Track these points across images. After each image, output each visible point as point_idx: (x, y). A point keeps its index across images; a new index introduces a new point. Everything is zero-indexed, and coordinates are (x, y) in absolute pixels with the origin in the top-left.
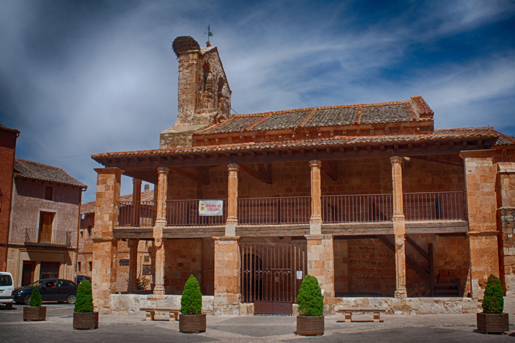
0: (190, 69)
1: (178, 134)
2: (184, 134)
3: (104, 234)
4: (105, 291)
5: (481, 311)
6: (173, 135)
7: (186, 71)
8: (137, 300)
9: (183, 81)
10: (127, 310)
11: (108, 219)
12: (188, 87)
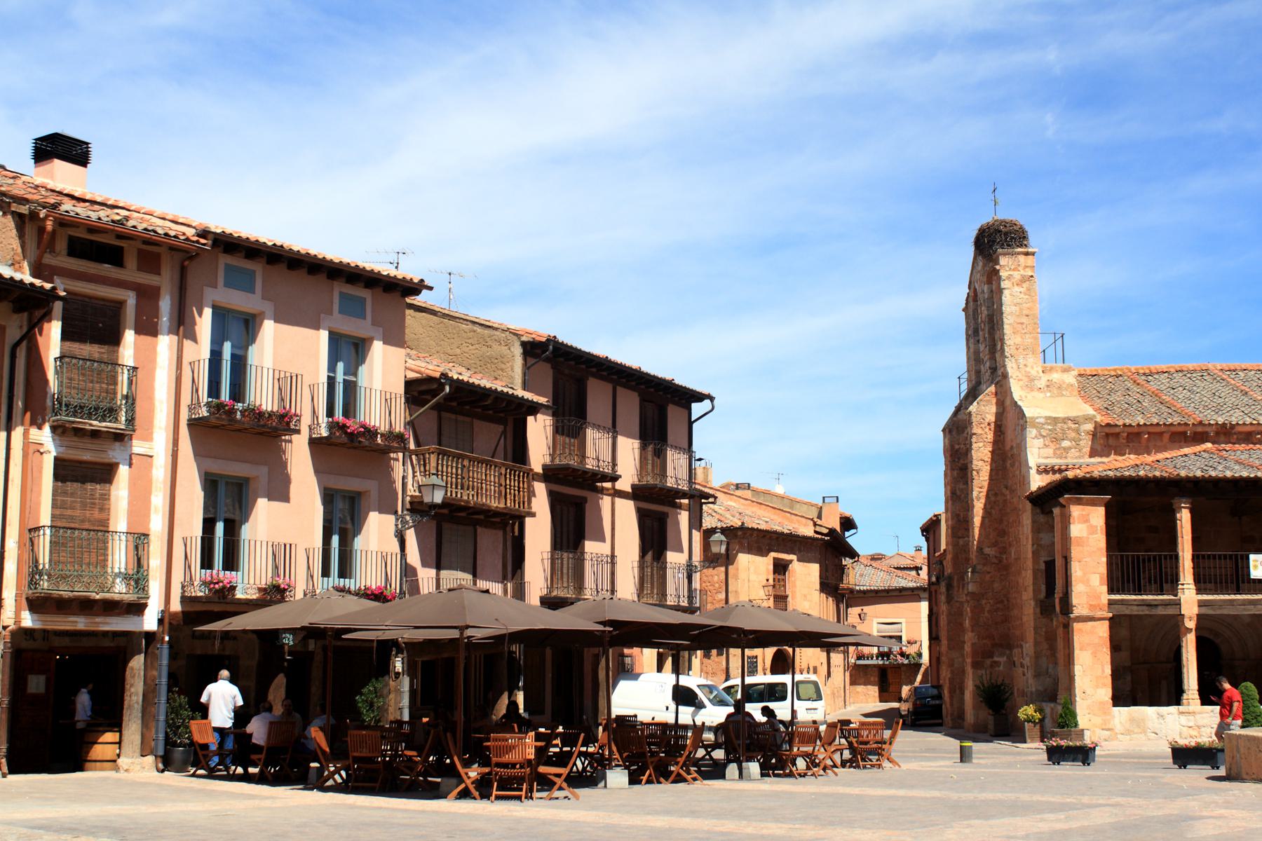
0: (1025, 285)
1: (1065, 420)
2: (1075, 420)
3: (1091, 607)
4: (1102, 703)
5: (754, 768)
6: (1055, 420)
7: (1017, 289)
8: (1161, 716)
9: (1013, 308)
10: (1144, 732)
11: (1097, 583)
12: (1024, 320)
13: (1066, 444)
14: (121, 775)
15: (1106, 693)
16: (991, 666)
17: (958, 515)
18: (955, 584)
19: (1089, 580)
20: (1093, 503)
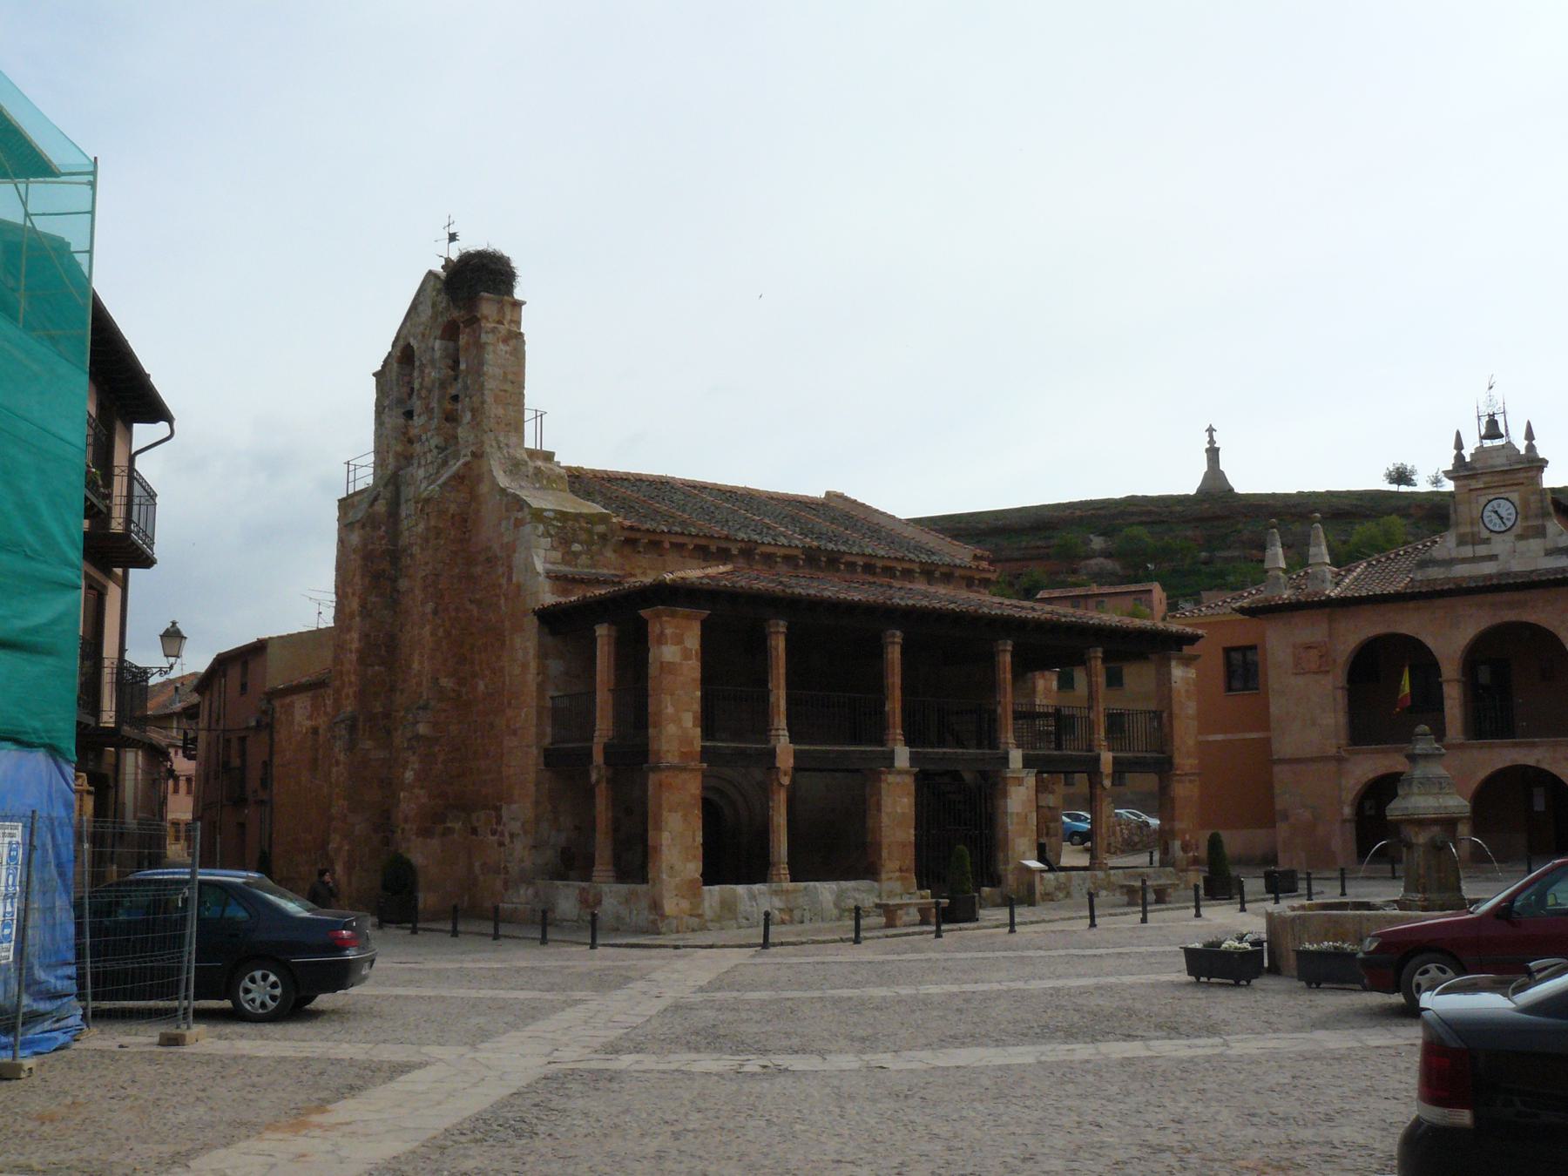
3: (684, 755)
4: (692, 881)
7: (501, 346)
11: (690, 724)
13: (576, 547)
14: (185, 1049)
15: (694, 869)
16: (443, 835)
17: (367, 636)
18: (360, 725)
19: (678, 722)
20: (688, 617)
